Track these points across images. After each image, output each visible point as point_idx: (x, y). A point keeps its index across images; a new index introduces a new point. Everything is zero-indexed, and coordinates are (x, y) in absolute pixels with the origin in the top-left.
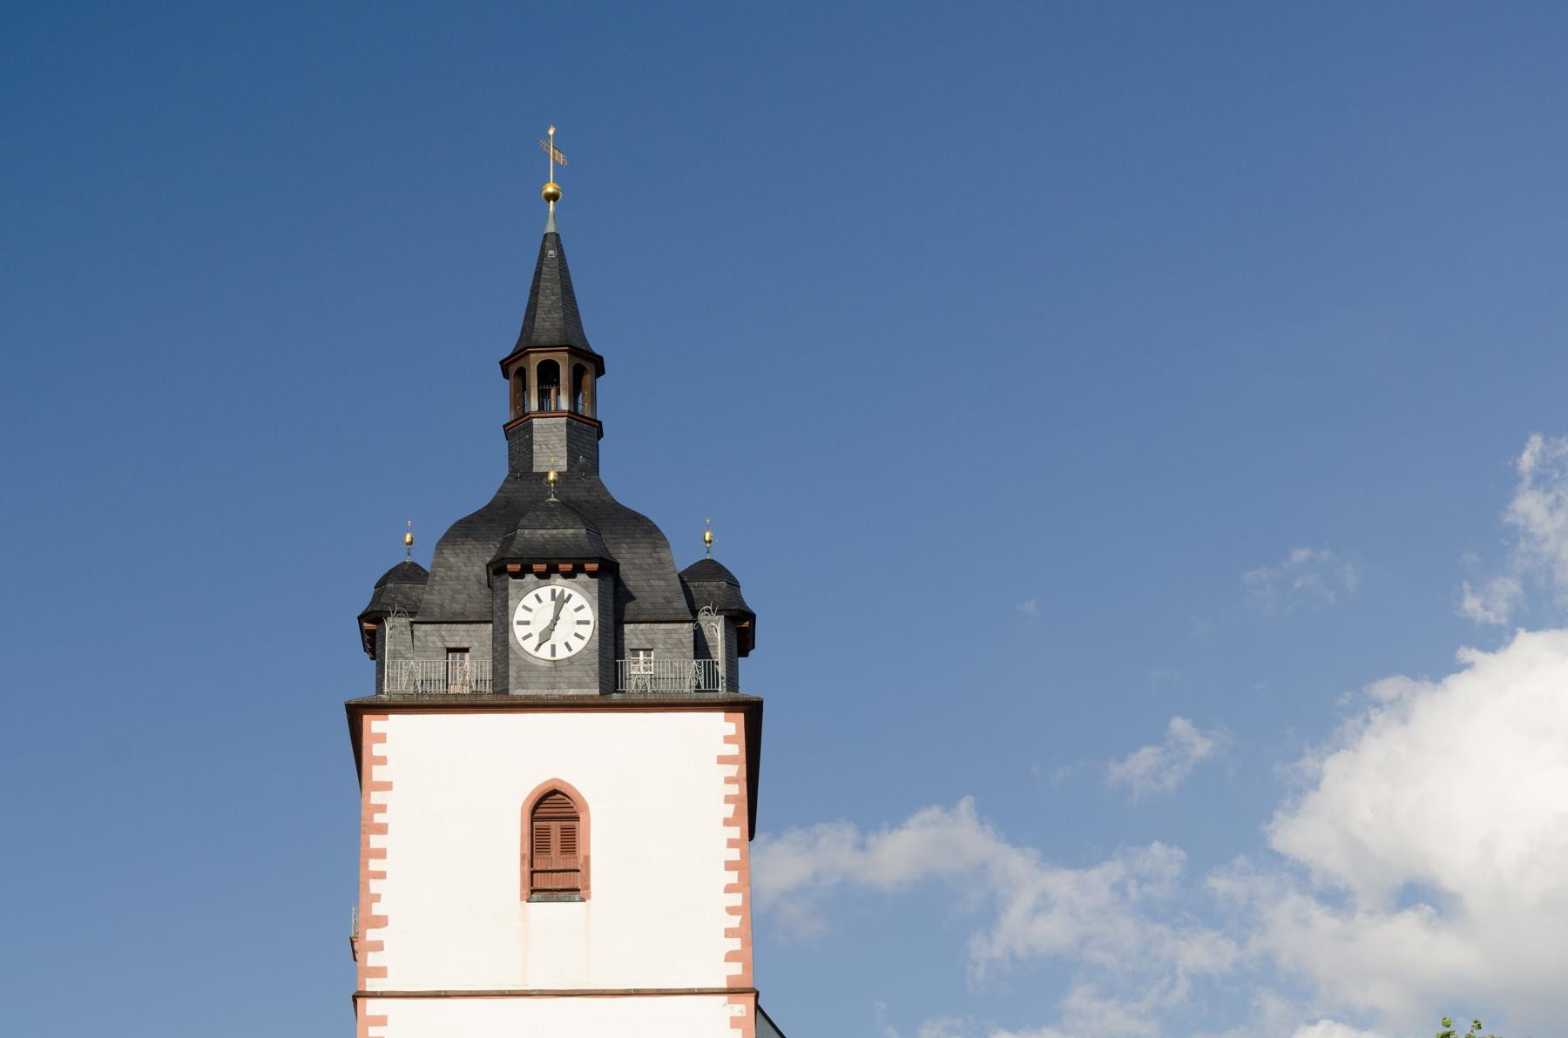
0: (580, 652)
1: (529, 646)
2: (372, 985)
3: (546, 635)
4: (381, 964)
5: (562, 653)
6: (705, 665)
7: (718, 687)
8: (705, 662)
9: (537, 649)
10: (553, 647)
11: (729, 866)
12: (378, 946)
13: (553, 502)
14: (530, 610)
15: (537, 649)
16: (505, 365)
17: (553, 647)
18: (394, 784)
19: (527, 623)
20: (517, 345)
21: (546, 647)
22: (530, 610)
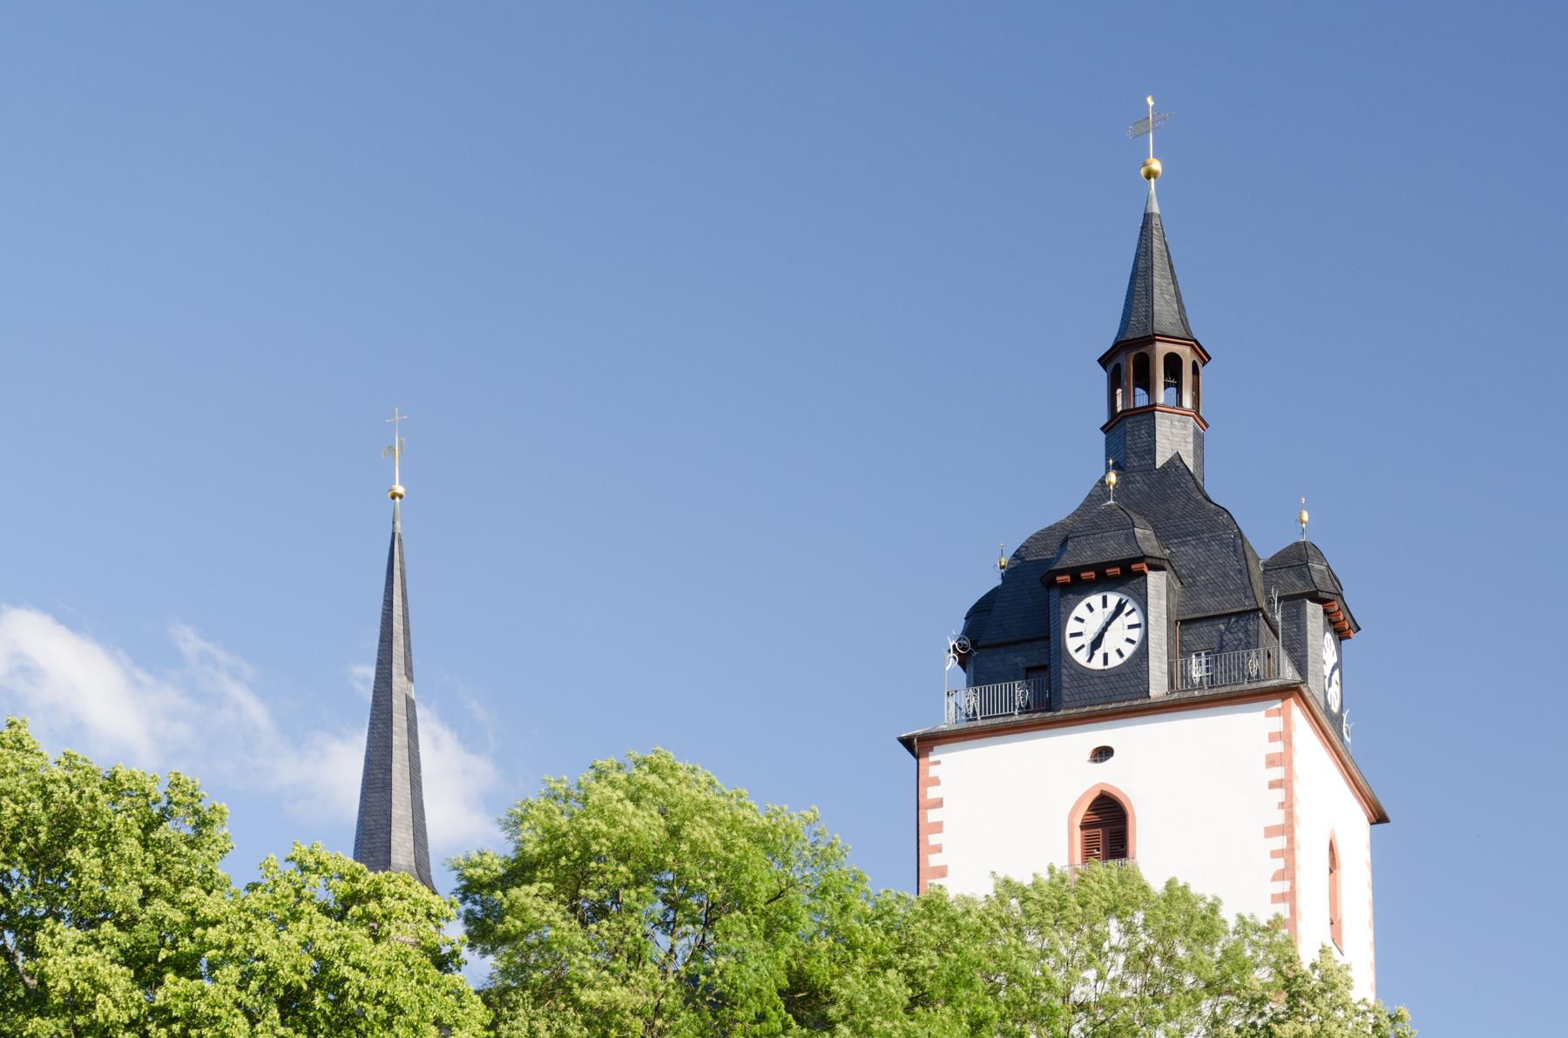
0: (1094, 670)
1: (1081, 658)
3: (1096, 643)
4: (942, 863)
5: (1115, 661)
6: (981, 691)
7: (1014, 710)
8: (981, 689)
9: (1089, 660)
10: (1106, 656)
11: (938, 827)
12: (938, 849)
13: (1140, 492)
14: (1081, 620)
15: (1089, 660)
16: (1104, 361)
17: (1106, 656)
18: (1263, 836)
19: (1080, 634)
20: (1116, 338)
21: (1099, 654)
22: (1081, 620)
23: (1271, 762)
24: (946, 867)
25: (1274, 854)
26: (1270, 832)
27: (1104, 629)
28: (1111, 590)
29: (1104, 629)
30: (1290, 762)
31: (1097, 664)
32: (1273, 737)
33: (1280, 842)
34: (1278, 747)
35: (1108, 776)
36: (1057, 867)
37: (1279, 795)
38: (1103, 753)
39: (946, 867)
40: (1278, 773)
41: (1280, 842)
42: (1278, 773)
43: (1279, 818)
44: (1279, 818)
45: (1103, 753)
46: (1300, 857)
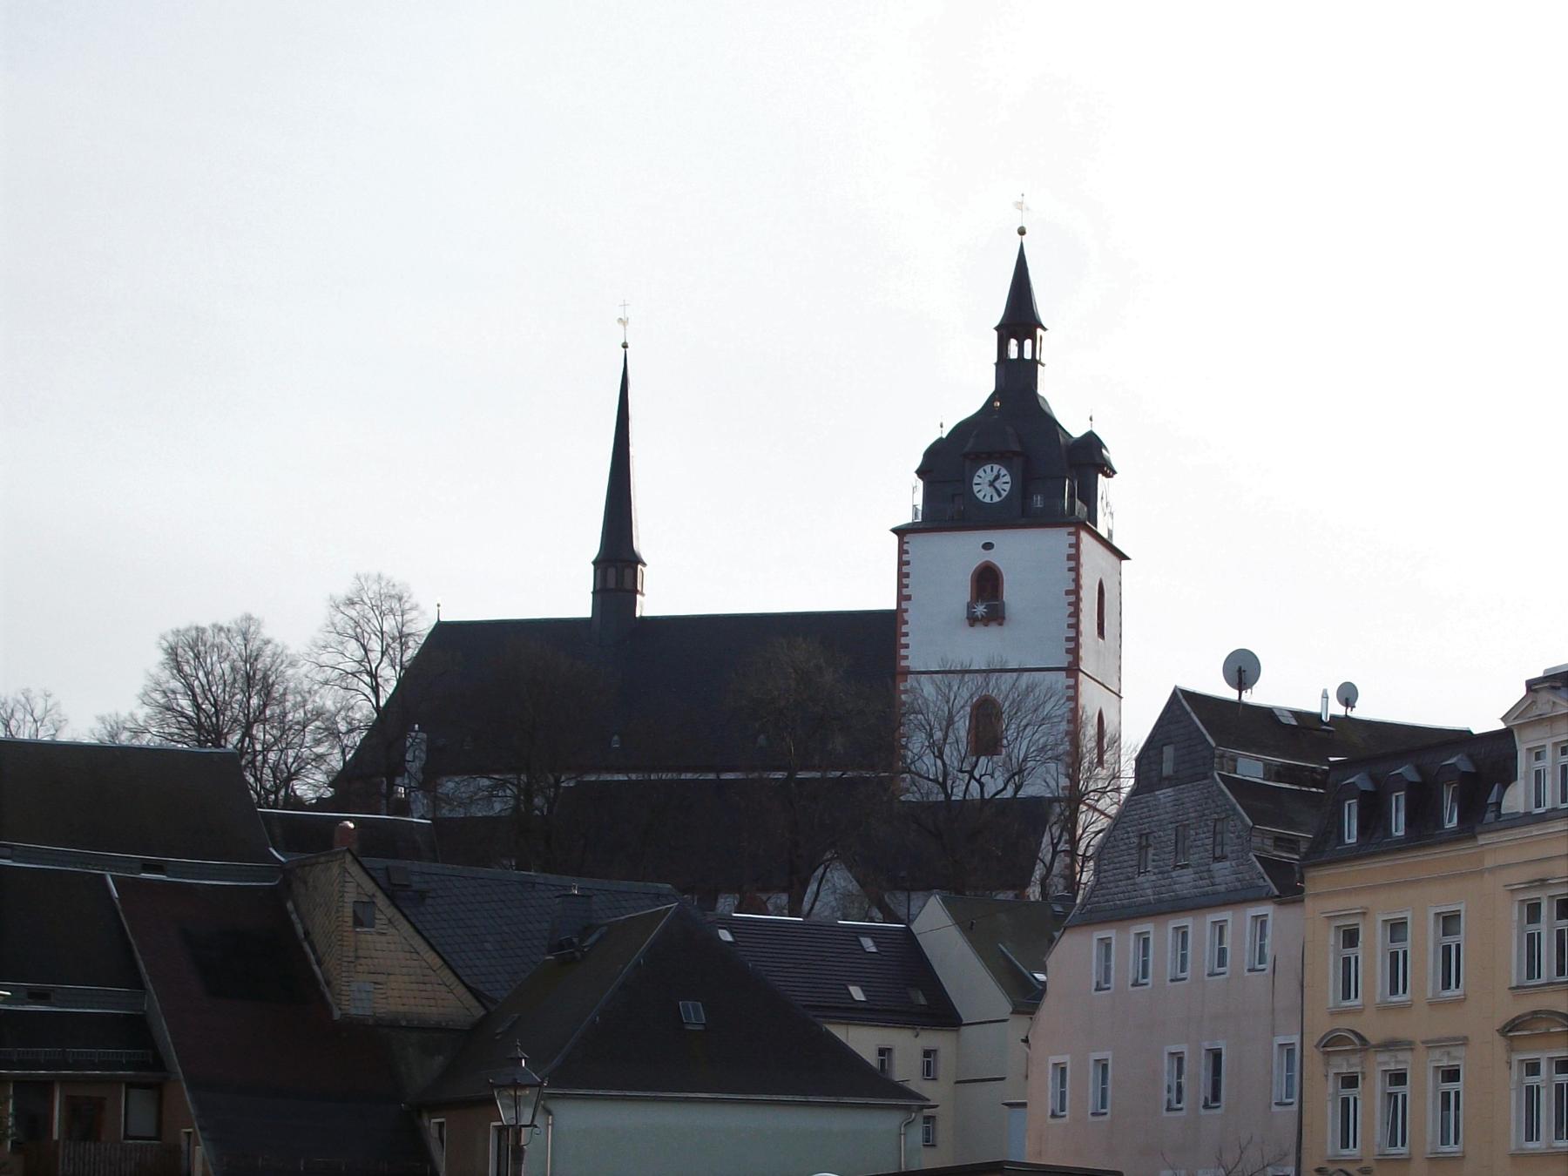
1: (1004, 471)
5: (988, 468)
23: (1070, 557)
24: (908, 644)
25: (1070, 604)
26: (1068, 593)
27: (160, 1112)
28: (985, 465)
29: (160, 1112)
30: (1079, 558)
31: (996, 467)
32: (1071, 546)
33: (1072, 598)
34: (1073, 551)
35: (990, 556)
36: (964, 663)
37: (1073, 575)
38: (988, 546)
39: (908, 644)
40: (1072, 564)
41: (1072, 598)
42: (1072, 564)
43: (1072, 587)
44: (1072, 587)
45: (988, 546)
46: (1083, 605)
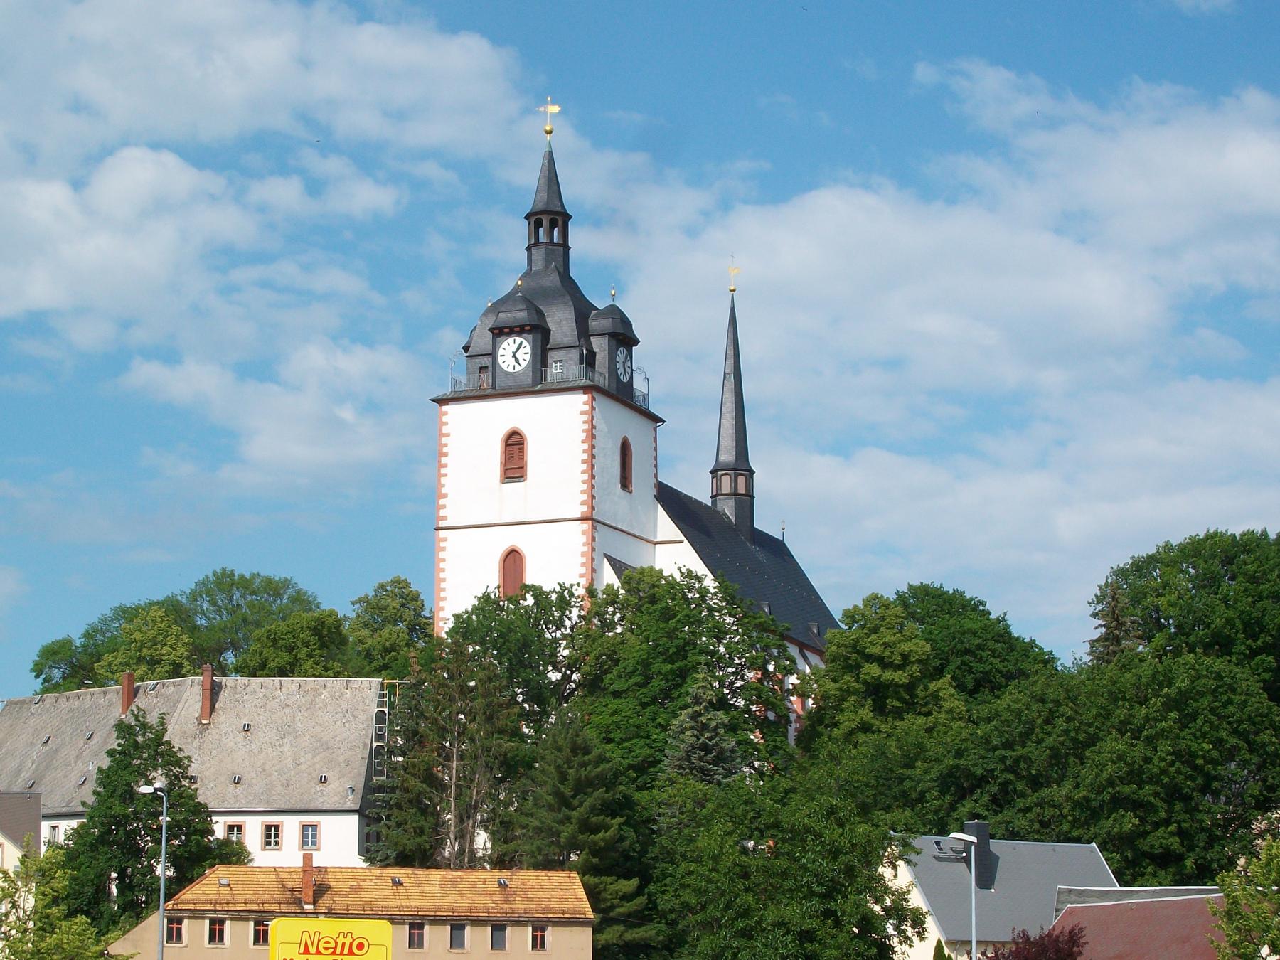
2: (442, 524)
